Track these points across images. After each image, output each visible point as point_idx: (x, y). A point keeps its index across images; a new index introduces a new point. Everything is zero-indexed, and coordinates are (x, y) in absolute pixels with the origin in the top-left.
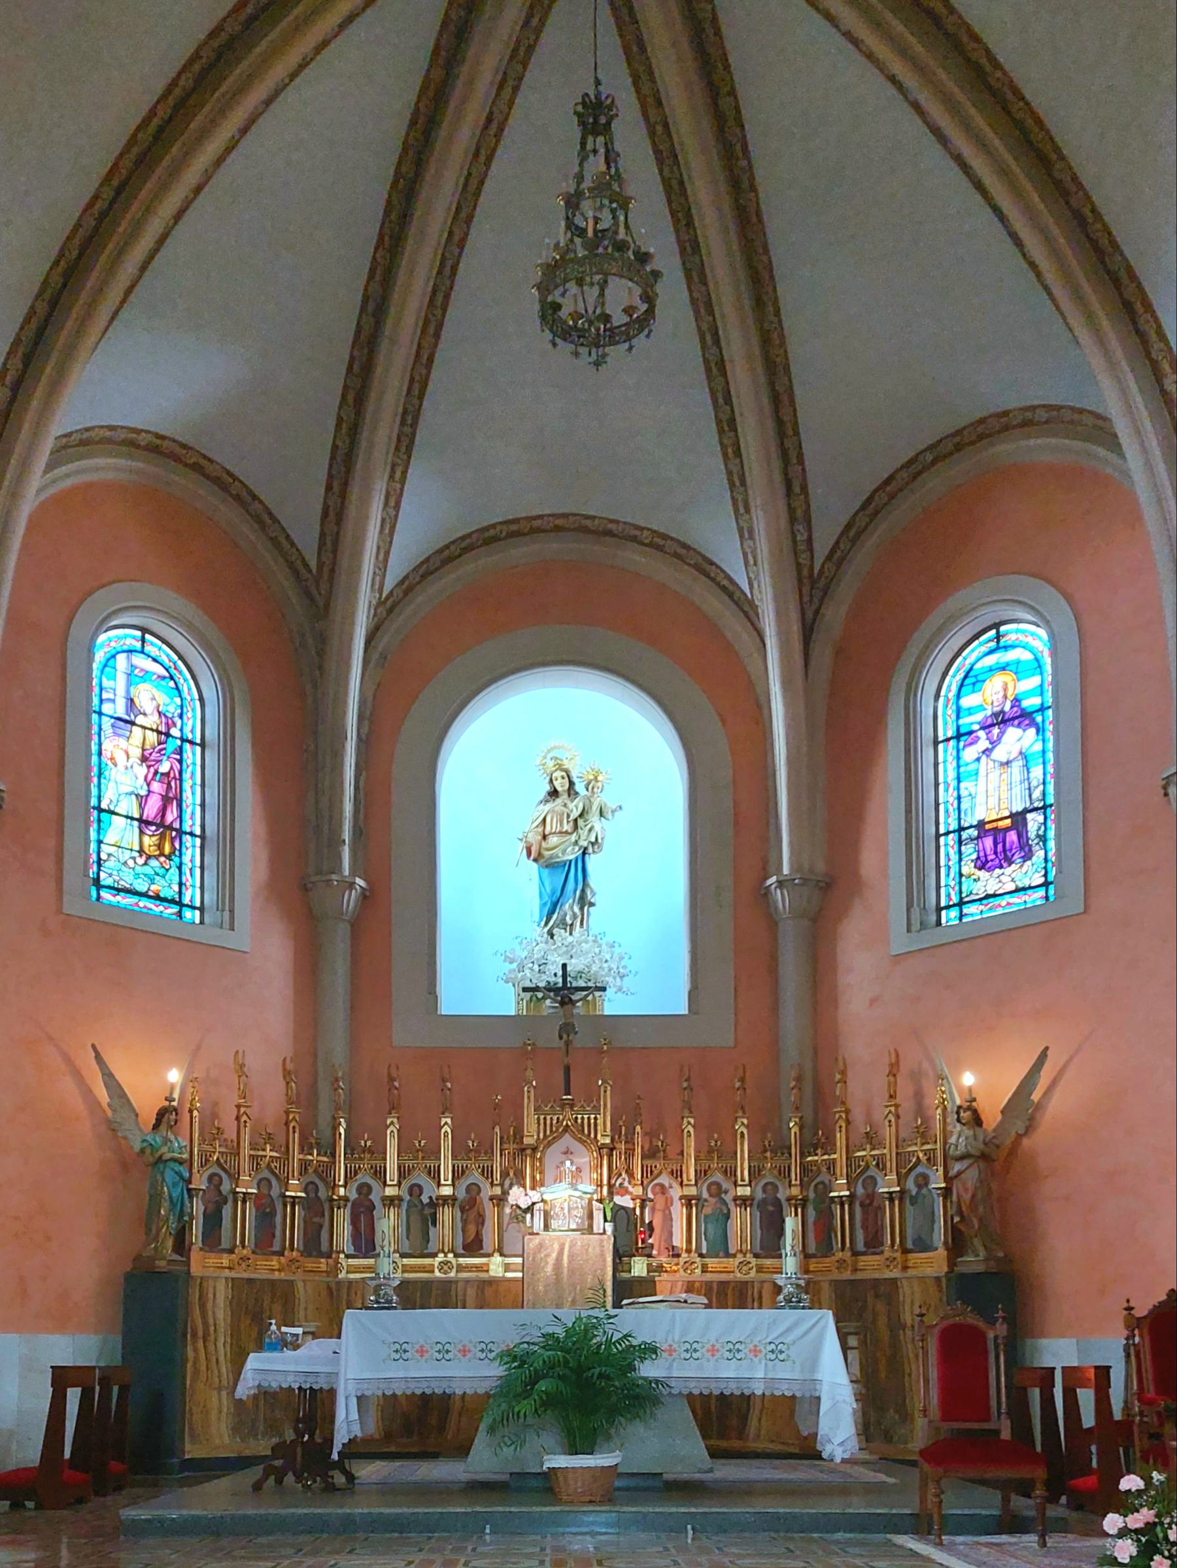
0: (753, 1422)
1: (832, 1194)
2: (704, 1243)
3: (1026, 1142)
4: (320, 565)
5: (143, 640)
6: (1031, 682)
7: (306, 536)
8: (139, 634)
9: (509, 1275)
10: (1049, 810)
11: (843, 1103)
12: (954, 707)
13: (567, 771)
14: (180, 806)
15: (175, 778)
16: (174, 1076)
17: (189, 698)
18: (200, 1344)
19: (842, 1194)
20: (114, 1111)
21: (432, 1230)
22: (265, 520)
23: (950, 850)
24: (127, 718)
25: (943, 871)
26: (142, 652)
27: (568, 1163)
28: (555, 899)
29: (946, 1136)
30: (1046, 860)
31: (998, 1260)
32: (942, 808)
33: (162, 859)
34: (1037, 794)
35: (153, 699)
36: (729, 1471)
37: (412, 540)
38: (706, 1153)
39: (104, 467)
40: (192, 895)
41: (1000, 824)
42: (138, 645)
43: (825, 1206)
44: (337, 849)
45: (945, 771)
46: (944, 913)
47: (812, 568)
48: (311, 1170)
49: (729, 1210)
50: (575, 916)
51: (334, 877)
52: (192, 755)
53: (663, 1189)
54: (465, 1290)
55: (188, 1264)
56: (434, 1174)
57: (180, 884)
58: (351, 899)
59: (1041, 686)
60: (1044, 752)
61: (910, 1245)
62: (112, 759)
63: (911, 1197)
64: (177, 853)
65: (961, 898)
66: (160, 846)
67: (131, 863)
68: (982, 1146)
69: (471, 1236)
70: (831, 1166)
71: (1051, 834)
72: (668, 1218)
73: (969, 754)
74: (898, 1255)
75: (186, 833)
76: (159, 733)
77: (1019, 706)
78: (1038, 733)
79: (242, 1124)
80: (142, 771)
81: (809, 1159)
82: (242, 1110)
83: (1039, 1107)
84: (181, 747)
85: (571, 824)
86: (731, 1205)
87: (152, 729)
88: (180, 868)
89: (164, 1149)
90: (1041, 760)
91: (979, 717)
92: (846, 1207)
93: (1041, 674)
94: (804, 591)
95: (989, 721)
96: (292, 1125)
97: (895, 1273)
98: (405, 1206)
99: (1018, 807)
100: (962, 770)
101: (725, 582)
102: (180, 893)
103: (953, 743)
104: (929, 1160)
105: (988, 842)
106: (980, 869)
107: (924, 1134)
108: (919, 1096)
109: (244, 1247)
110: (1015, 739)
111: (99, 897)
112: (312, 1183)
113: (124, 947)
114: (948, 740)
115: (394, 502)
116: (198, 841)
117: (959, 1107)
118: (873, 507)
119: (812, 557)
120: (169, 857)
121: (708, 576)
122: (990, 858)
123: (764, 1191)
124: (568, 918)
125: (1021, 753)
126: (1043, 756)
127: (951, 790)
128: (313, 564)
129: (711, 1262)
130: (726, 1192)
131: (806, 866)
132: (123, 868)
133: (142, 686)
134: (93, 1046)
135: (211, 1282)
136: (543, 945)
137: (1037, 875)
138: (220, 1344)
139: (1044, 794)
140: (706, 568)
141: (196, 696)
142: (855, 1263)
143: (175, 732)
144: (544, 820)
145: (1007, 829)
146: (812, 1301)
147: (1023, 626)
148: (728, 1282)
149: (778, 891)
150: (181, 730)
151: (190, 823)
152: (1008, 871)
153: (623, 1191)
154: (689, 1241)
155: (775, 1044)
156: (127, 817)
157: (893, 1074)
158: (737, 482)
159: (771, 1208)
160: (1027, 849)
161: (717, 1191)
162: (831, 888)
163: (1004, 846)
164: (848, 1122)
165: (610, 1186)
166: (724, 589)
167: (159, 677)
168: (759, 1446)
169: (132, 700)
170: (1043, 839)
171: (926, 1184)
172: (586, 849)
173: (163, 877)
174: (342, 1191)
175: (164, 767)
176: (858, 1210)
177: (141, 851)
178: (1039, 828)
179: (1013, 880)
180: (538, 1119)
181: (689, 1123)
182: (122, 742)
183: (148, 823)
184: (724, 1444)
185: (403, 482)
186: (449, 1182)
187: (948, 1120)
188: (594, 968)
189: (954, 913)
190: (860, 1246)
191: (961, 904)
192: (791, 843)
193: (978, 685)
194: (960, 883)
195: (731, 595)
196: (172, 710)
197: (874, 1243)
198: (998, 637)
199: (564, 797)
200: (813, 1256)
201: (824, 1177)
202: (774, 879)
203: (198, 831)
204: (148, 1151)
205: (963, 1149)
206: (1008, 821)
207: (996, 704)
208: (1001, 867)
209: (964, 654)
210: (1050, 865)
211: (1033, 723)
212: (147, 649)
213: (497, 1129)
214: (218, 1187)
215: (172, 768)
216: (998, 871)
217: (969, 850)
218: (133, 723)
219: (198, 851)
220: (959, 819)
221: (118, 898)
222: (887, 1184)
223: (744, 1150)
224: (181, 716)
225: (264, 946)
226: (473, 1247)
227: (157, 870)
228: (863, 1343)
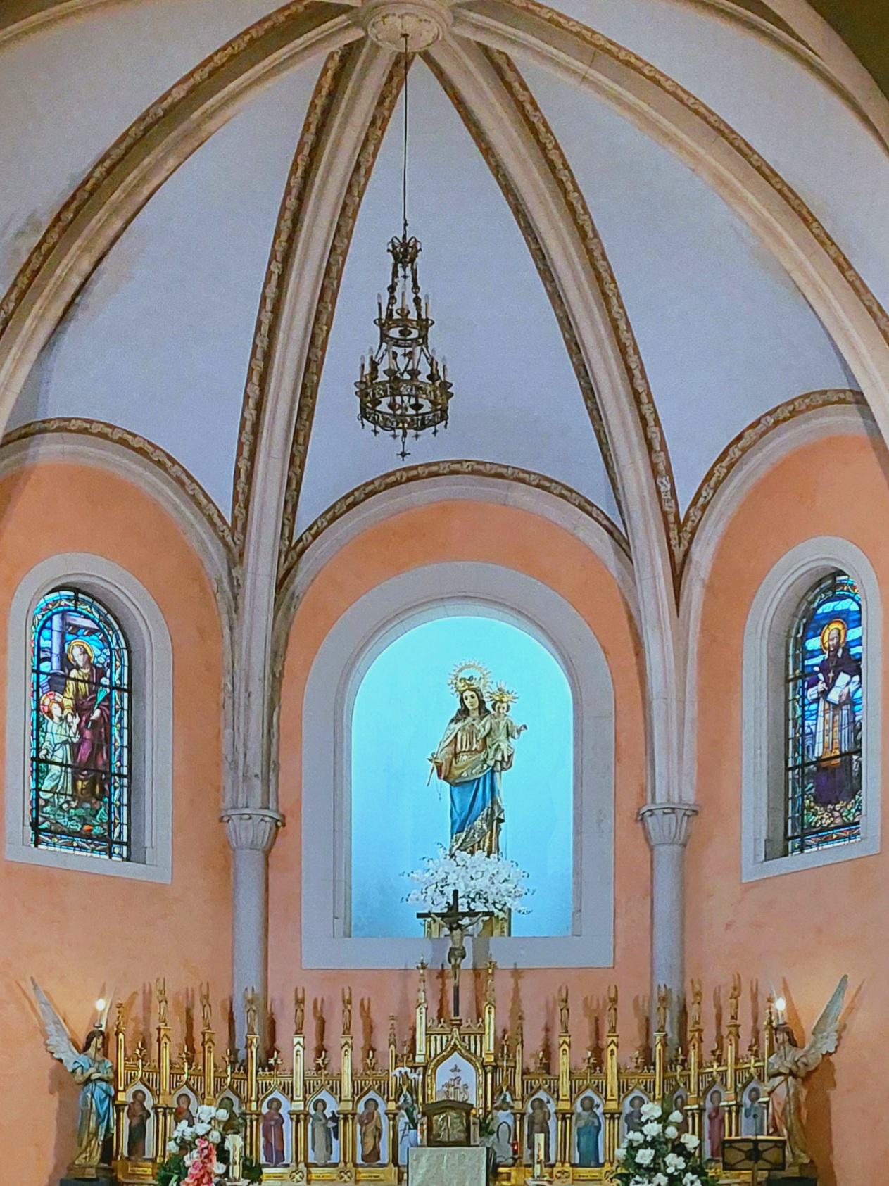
4: (234, 518)
5: (76, 599)
16: (101, 1005)
22: (183, 481)
26: (75, 611)
31: (802, 1166)
69: (370, 1147)
82: (162, 1032)
89: (92, 1070)
91: (818, 660)
94: (671, 535)
104: (759, 1076)
130: (598, 1106)
134: (32, 978)
143: (105, 681)
144: (456, 737)
150: (110, 679)
174: (254, 1106)
176: (706, 1121)
182: (58, 697)
204: (79, 1070)
222: (728, 1100)
224: (110, 665)
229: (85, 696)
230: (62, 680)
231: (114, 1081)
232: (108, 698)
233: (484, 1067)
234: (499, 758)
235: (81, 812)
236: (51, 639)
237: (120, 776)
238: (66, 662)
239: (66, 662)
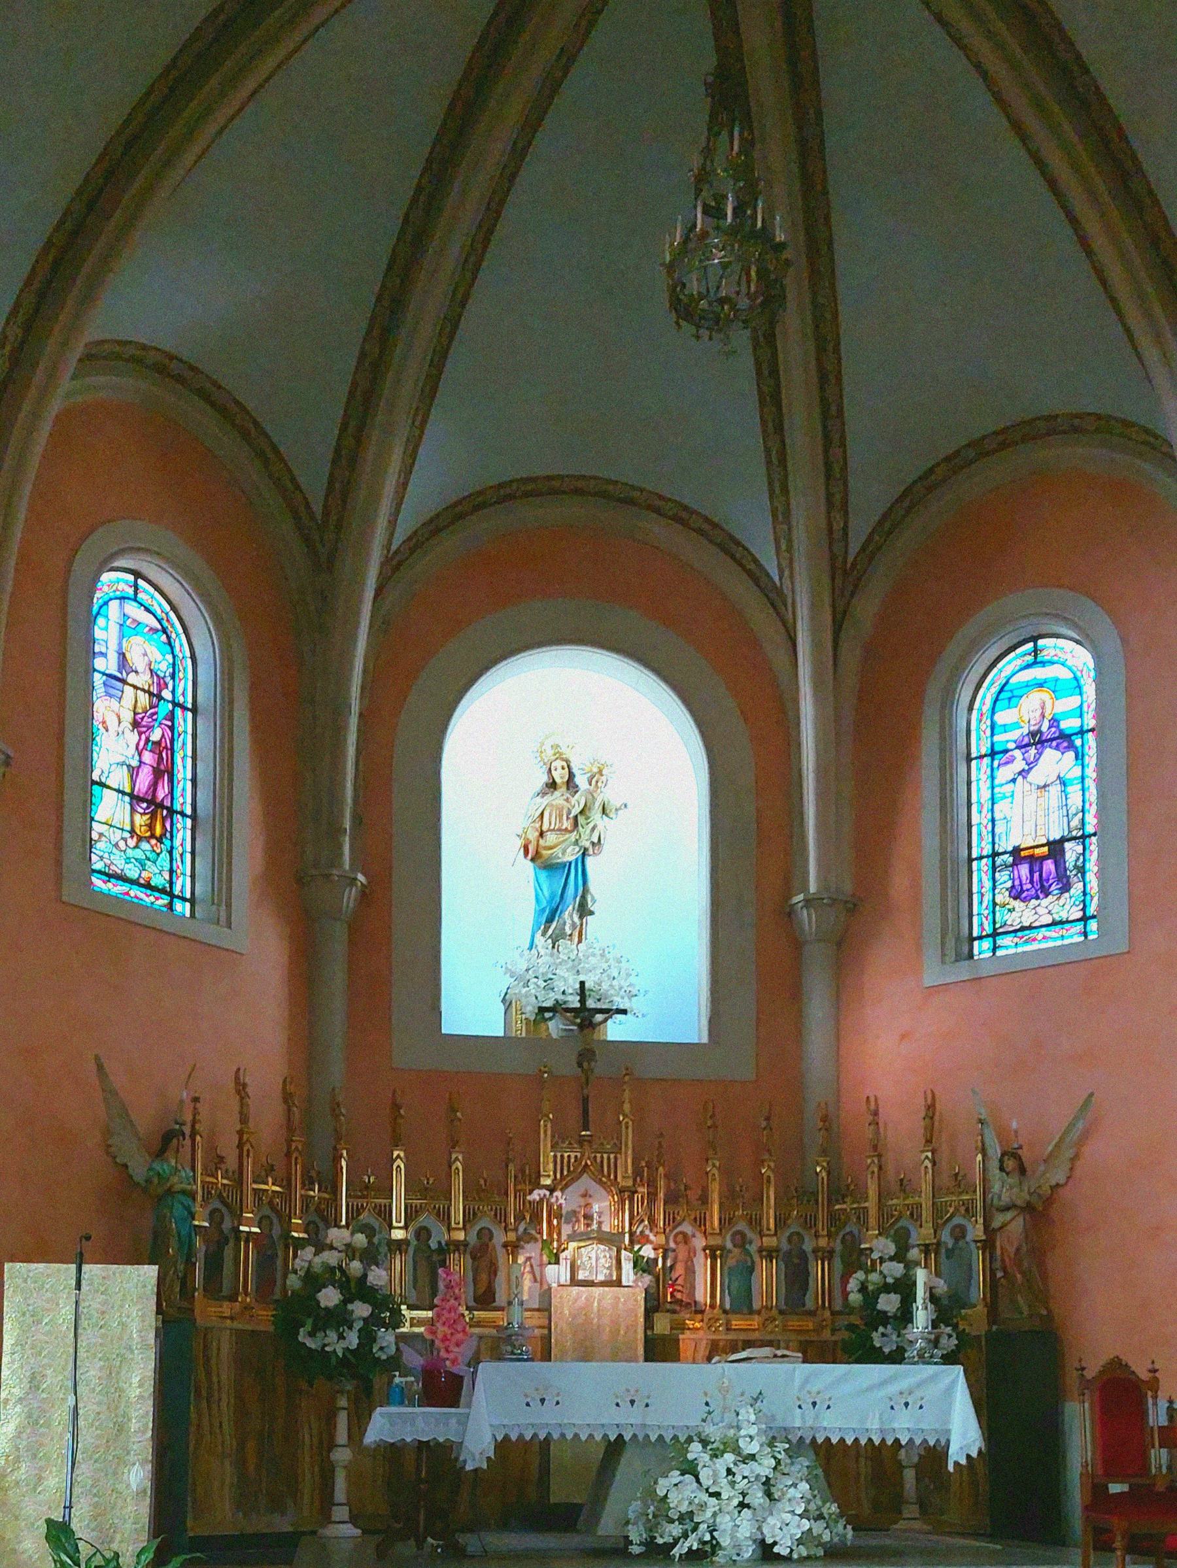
1: (862, 1246)
2: (727, 1299)
4: (326, 512)
7: (313, 480)
8: (131, 578)
12: (989, 723)
13: (567, 761)
14: (171, 781)
15: (166, 747)
17: (181, 656)
18: (204, 1404)
22: (268, 454)
23: (983, 875)
24: (119, 675)
25: (976, 898)
26: (135, 600)
28: (554, 905)
32: (974, 830)
33: (153, 841)
34: (1075, 822)
35: (145, 654)
37: (427, 492)
38: (730, 1198)
39: (108, 386)
40: (182, 885)
41: (1037, 851)
42: (131, 591)
44: (341, 841)
45: (979, 790)
47: (845, 558)
48: (312, 1209)
49: (753, 1262)
50: (574, 925)
51: (335, 872)
52: (184, 722)
53: (686, 1239)
56: (444, 1217)
57: (171, 871)
58: (350, 897)
59: (1081, 707)
63: (947, 1250)
64: (168, 835)
65: (995, 929)
66: (151, 827)
67: (122, 844)
68: (1028, 1197)
72: (690, 1271)
73: (1005, 773)
75: (178, 813)
76: (151, 694)
77: (1058, 727)
78: (1077, 758)
79: (245, 1153)
80: (133, 737)
81: (837, 1207)
84: (172, 712)
85: (571, 821)
86: (757, 1259)
87: (143, 690)
88: (171, 853)
90: (1080, 786)
91: (1015, 735)
93: (1081, 694)
95: (1026, 740)
96: (294, 1155)
100: (996, 791)
101: (752, 566)
102: (171, 883)
103: (987, 760)
105: (1024, 870)
106: (1015, 898)
107: (959, 1181)
109: (246, 1294)
110: (1053, 762)
112: (314, 1222)
114: (981, 757)
116: (189, 822)
118: (911, 499)
119: (846, 546)
120: (160, 840)
121: (733, 557)
122: (1025, 887)
123: (789, 1240)
125: (1059, 777)
126: (1083, 782)
127: (985, 811)
128: (318, 509)
129: (736, 1323)
130: (751, 1243)
132: (114, 850)
133: (134, 640)
136: (548, 958)
137: (1075, 909)
138: (224, 1404)
140: (732, 548)
141: (188, 654)
143: (166, 694)
144: (542, 814)
145: (1043, 858)
149: (805, 912)
150: (173, 692)
151: (181, 800)
152: (1045, 902)
153: (644, 1240)
154: (713, 1296)
156: (119, 791)
158: (777, 461)
159: (796, 1261)
160: (1065, 881)
161: (741, 1241)
162: (858, 913)
163: (1041, 876)
165: (632, 1234)
166: (750, 573)
167: (151, 629)
169: (124, 655)
170: (1082, 870)
171: (964, 1237)
173: (155, 862)
175: (156, 735)
177: (132, 832)
178: (1078, 859)
180: (555, 1156)
181: (714, 1165)
182: (114, 703)
188: (605, 986)
189: (987, 944)
191: (995, 934)
192: (819, 861)
193: (1014, 700)
194: (994, 912)
195: (757, 582)
196: (164, 669)
198: (1036, 651)
202: (801, 897)
203: (188, 811)
205: (1008, 1199)
206: (1046, 849)
207: (1032, 722)
208: (1037, 898)
209: (1000, 665)
211: (1071, 746)
212: (140, 596)
215: (163, 735)
216: (1034, 902)
217: (1003, 877)
218: (124, 682)
219: (189, 833)
220: (994, 843)
221: (110, 885)
224: (173, 676)
227: (148, 854)
230: (119, 685)
232: (171, 716)
235: (138, 854)
236: (106, 629)
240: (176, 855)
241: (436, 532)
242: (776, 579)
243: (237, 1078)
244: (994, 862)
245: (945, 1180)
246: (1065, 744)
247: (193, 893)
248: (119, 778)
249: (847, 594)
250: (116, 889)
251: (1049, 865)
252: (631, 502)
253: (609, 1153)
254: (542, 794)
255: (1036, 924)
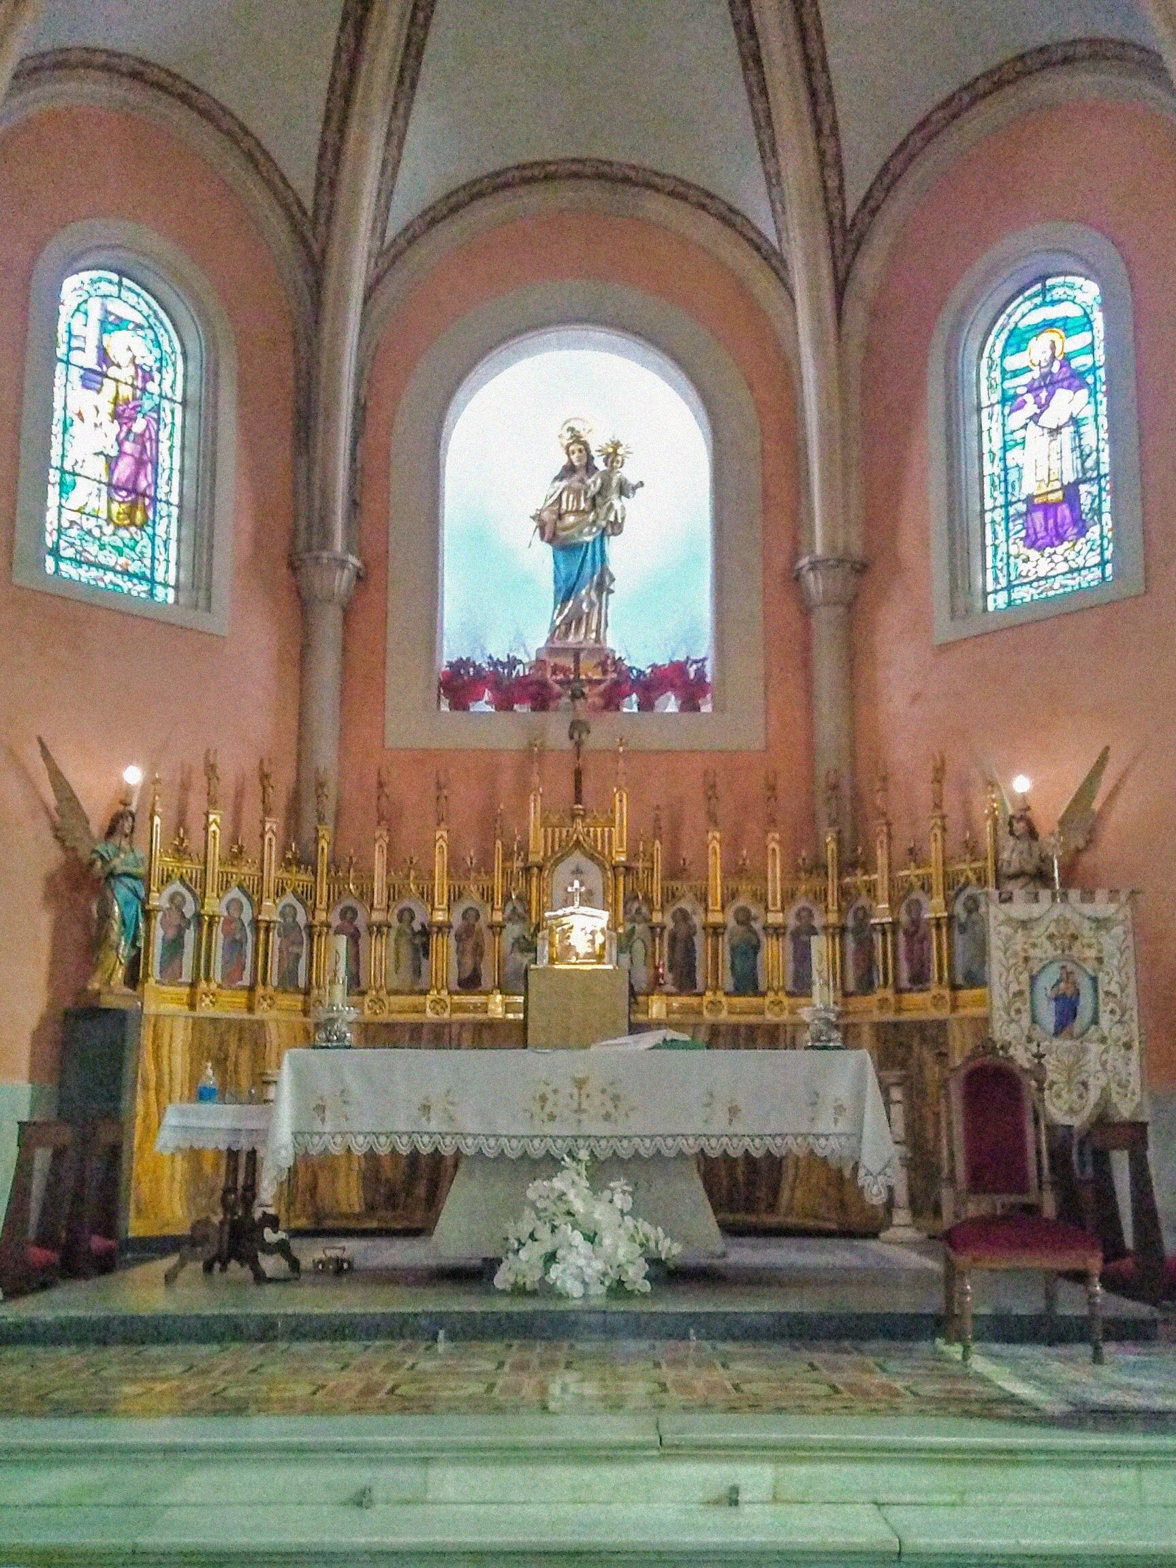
0: (785, 1195)
1: (873, 921)
3: (1085, 859)
5: (120, 284)
6: (1079, 341)
9: (510, 1016)
10: (1103, 482)
11: (884, 814)
13: (585, 444)
16: (133, 775)
19: (884, 920)
20: (62, 816)
21: (424, 961)
22: (256, 157)
27: (577, 884)
29: (997, 853)
30: (1102, 537)
33: (133, 529)
34: (1090, 463)
36: (748, 1254)
43: (863, 932)
46: (991, 598)
47: (843, 219)
51: (325, 554)
54: (460, 1034)
55: (141, 998)
56: (427, 896)
58: (342, 581)
60: (1096, 415)
61: (960, 980)
62: (80, 414)
66: (130, 515)
70: (871, 888)
71: (1106, 506)
74: (946, 993)
83: (1100, 816)
91: (1026, 379)
92: (889, 939)
93: (1092, 329)
97: (943, 1014)
98: (393, 933)
99: (1069, 478)
102: (153, 569)
104: (979, 879)
105: (1038, 516)
106: (1030, 547)
107: (972, 848)
108: (966, 804)
110: (1066, 403)
111: (57, 569)
113: (79, 621)
115: (395, 139)
117: (1012, 817)
118: (904, 155)
120: (141, 528)
123: (798, 915)
124: (584, 605)
125: (1072, 418)
128: (308, 204)
131: (840, 546)
134: (40, 740)
135: (168, 1020)
139: (1098, 463)
140: (730, 217)
142: (899, 1002)
143: (152, 387)
145: (1056, 504)
146: (844, 1039)
147: (1070, 279)
148: (758, 1026)
151: (167, 489)
152: (1060, 549)
155: (810, 747)
157: (938, 781)
162: (865, 572)
164: (890, 837)
168: (792, 1220)
170: (1099, 512)
171: (977, 908)
172: (604, 530)
173: (133, 549)
176: (902, 938)
177: (109, 520)
179: (1066, 560)
183: (117, 488)
184: (741, 1217)
185: (406, 117)
186: (444, 906)
187: (1000, 833)
190: (905, 983)
194: (1008, 564)
195: (758, 249)
197: (919, 979)
198: (1044, 291)
199: (582, 473)
200: (852, 994)
201: (863, 901)
208: (1052, 545)
210: (1105, 542)
213: (499, 843)
214: (179, 909)
216: (1049, 550)
222: (934, 908)
223: (775, 870)
224: (160, 370)
225: (249, 636)
226: (471, 983)
228: (908, 1096)
229: (127, 402)
231: (146, 879)
233: (614, 868)
234: (612, 518)
237: (168, 503)
238: (104, 356)
239: (104, 356)
240: (158, 541)
241: (433, 222)
242: (776, 244)
243: (206, 757)
244: (1007, 512)
245: (954, 847)
246: (1077, 383)
247: (177, 580)
248: (97, 468)
249: (849, 254)
250: (85, 575)
251: (1064, 510)
252: (626, 180)
253: (554, 827)
254: (559, 478)
255: (1053, 573)
